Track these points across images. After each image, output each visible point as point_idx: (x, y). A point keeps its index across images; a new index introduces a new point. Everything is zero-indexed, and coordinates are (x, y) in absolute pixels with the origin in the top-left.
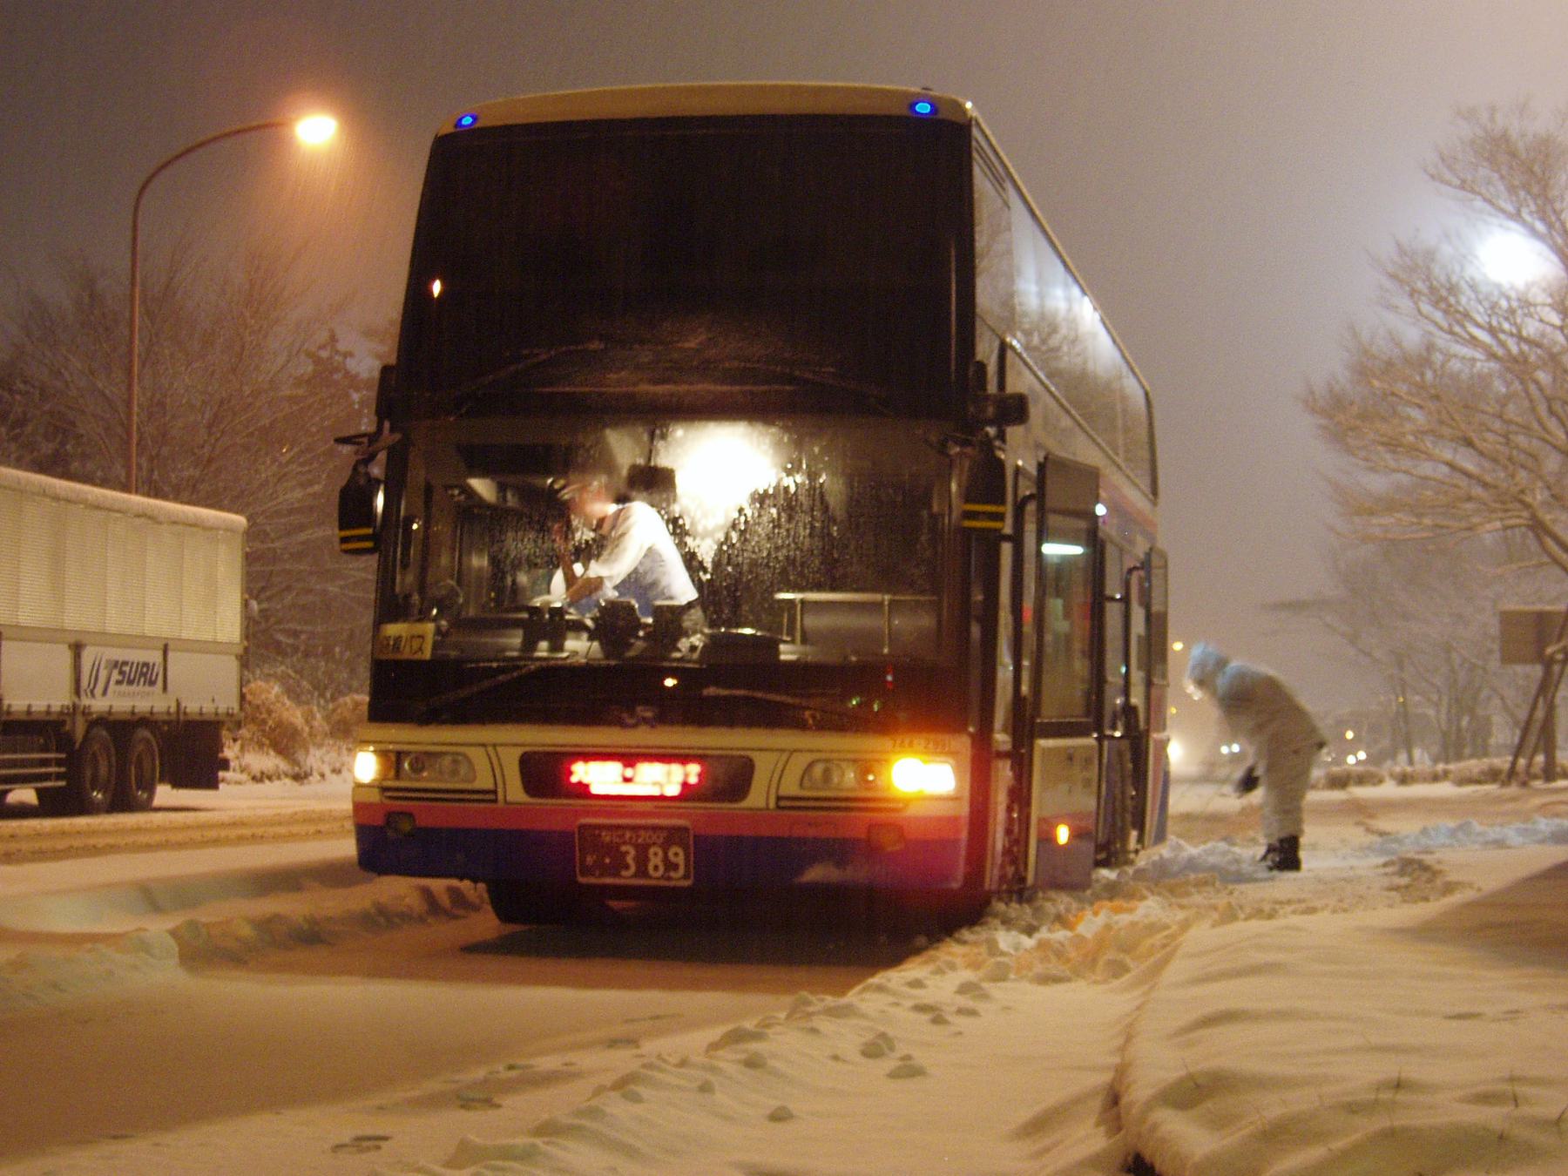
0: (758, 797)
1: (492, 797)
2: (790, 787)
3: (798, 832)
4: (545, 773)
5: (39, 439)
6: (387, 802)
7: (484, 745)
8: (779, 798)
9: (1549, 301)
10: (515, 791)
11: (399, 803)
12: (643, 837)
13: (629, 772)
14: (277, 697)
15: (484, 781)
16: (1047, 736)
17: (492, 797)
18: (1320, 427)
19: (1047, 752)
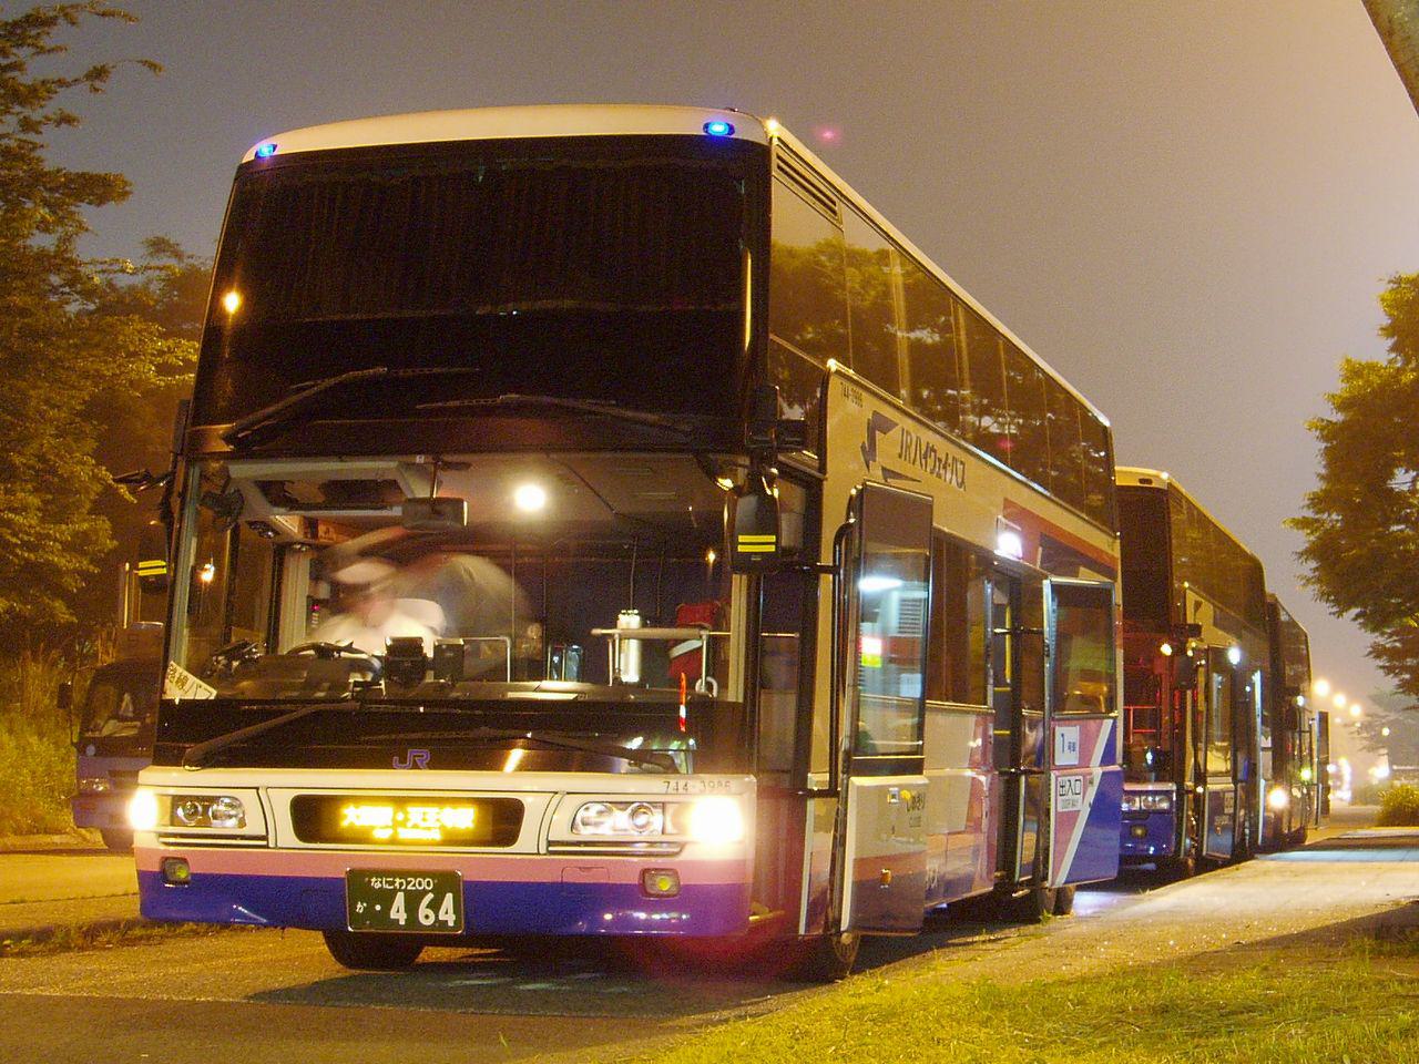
0: (528, 839)
1: (264, 843)
2: (561, 832)
3: (570, 878)
4: (311, 816)
5: (1214, 547)
6: (163, 847)
7: (257, 789)
8: (550, 843)
9: (1307, 502)
10: (285, 835)
11: (172, 848)
12: (414, 884)
13: (400, 817)
14: (653, 652)
15: (255, 826)
16: (859, 774)
17: (264, 843)
18: (1378, 652)
19: (861, 789)
